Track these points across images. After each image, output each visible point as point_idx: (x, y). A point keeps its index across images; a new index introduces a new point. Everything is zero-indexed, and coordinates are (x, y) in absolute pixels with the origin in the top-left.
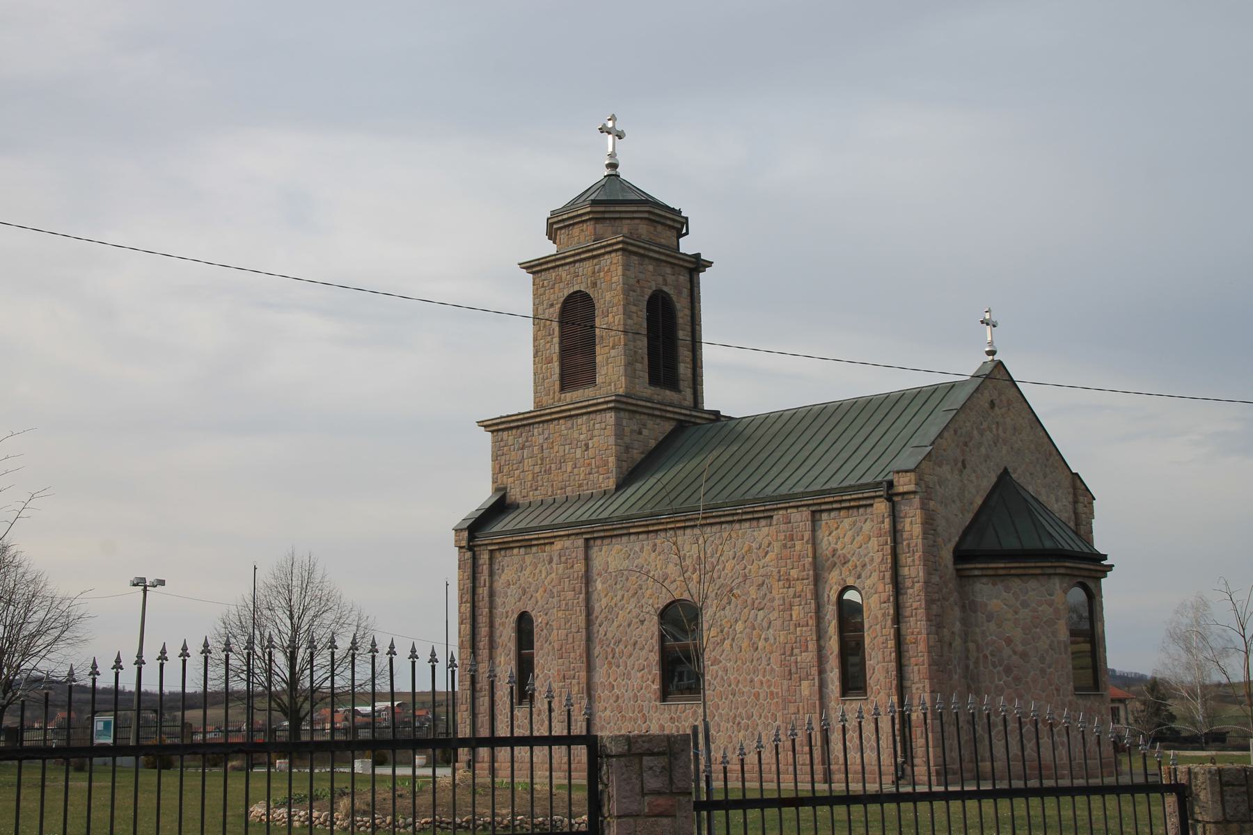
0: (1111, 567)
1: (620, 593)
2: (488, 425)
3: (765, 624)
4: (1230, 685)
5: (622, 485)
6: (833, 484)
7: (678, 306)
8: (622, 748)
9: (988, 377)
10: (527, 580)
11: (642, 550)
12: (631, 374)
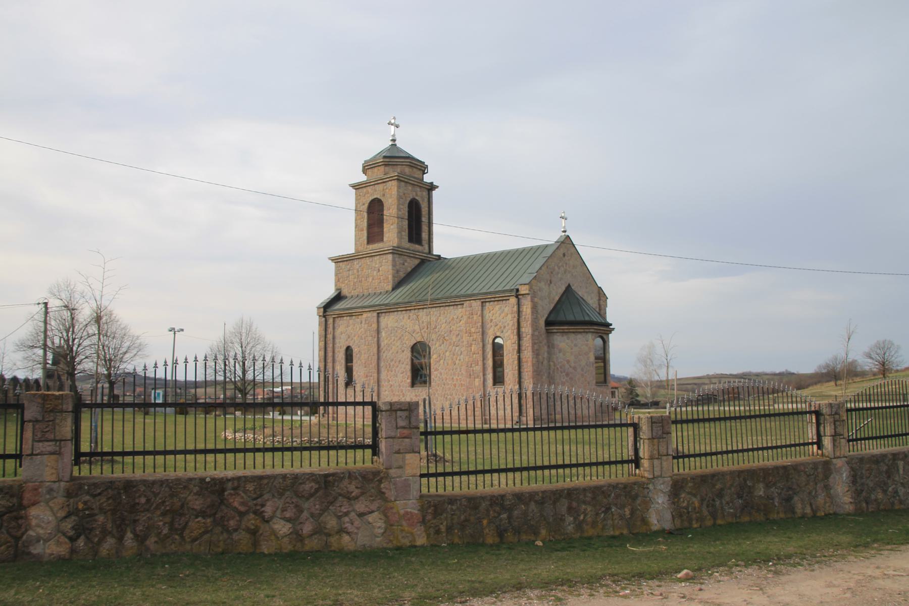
0: (613, 329)
4: (661, 381)
5: (396, 287)
6: (492, 290)
7: (423, 206)
8: (388, 407)
9: (563, 242)
10: (350, 331)
12: (400, 237)
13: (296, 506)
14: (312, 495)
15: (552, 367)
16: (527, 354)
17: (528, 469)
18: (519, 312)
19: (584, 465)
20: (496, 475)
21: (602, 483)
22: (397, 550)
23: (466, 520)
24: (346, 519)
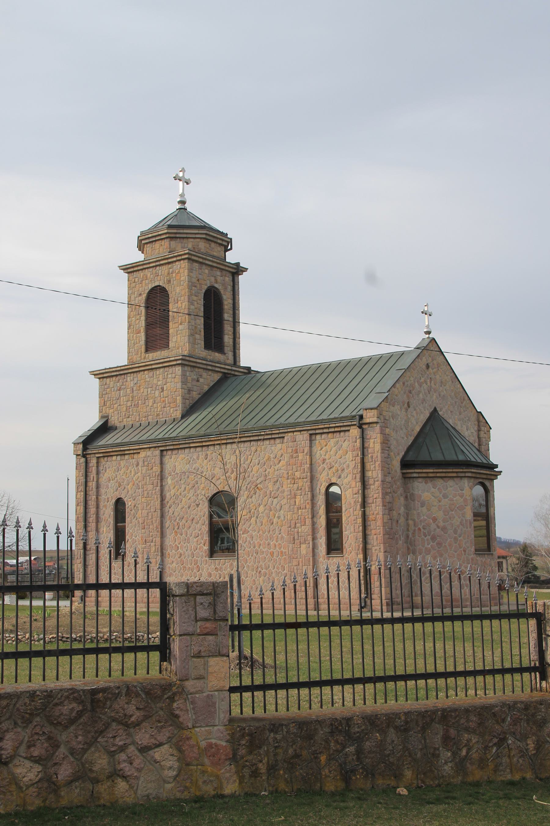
1: (183, 487)
3: (278, 507)
6: (324, 416)
7: (224, 297)
8: (183, 591)
10: (122, 477)
11: (198, 458)
12: (193, 343)
13: (49, 738)
14: (72, 722)
15: (412, 528)
16: (376, 509)
17: (385, 679)
18: (363, 448)
19: (465, 674)
20: (337, 689)
21: (492, 701)
22: (196, 802)
23: (297, 756)
24: (123, 756)
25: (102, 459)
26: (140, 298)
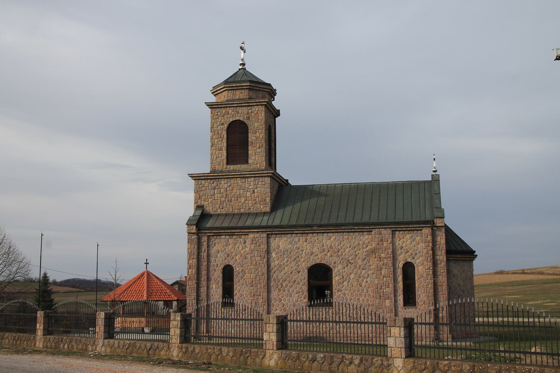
1: (286, 260)
2: (192, 176)
10: (223, 250)
25: (212, 237)
26: (222, 126)
